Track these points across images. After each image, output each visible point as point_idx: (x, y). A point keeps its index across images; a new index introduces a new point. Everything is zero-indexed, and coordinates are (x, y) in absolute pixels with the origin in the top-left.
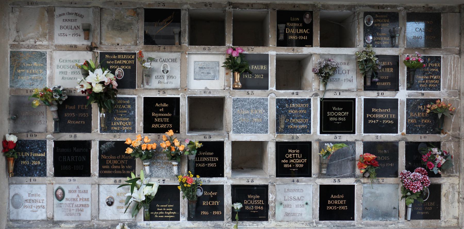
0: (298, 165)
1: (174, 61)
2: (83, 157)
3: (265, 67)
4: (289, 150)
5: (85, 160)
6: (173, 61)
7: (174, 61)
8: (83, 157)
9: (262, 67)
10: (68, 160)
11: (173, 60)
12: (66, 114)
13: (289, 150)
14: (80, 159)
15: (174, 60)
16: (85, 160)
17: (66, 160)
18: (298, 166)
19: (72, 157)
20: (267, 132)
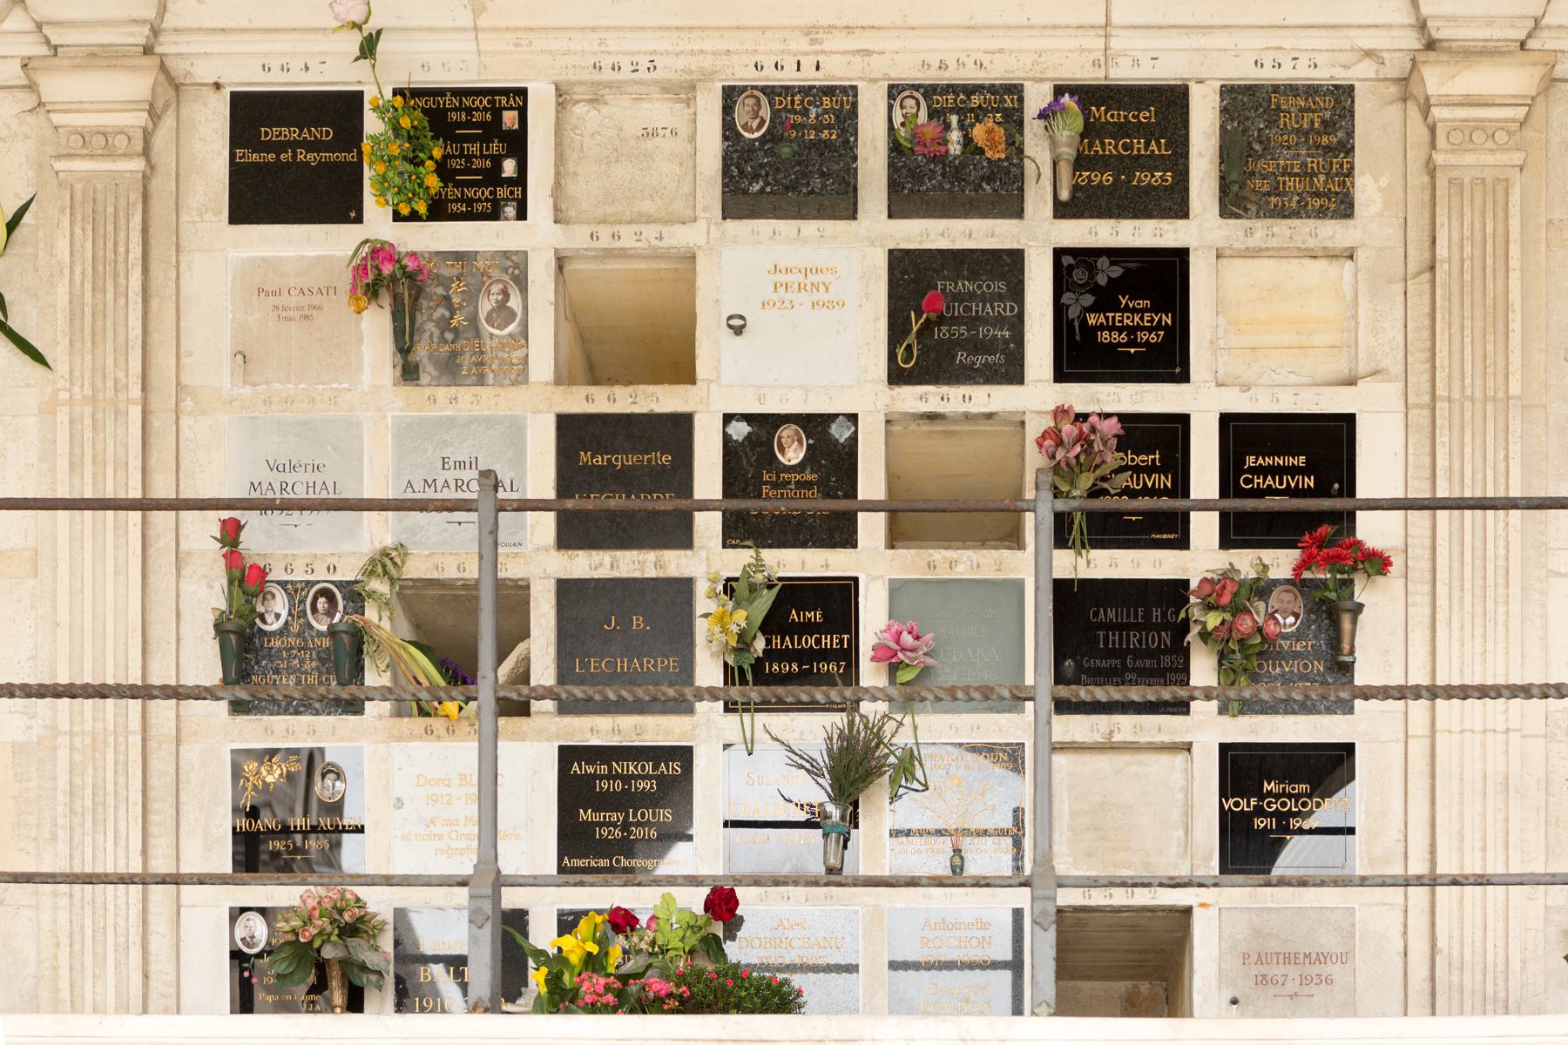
0: (1262, 822)
1: (1292, 962)
2: (1163, 633)
3: (674, 662)
4: (1266, 784)
5: (1168, 643)
6: (1287, 960)
7: (1292, 962)
8: (1163, 633)
9: (475, 592)
10: (787, 646)
11: (1287, 955)
12: (939, 331)
13: (1266, 784)
14: (1153, 637)
15: (1292, 955)
16: (1168, 643)
17: (782, 645)
18: (1262, 825)
19: (1132, 633)
20: (684, 754)
